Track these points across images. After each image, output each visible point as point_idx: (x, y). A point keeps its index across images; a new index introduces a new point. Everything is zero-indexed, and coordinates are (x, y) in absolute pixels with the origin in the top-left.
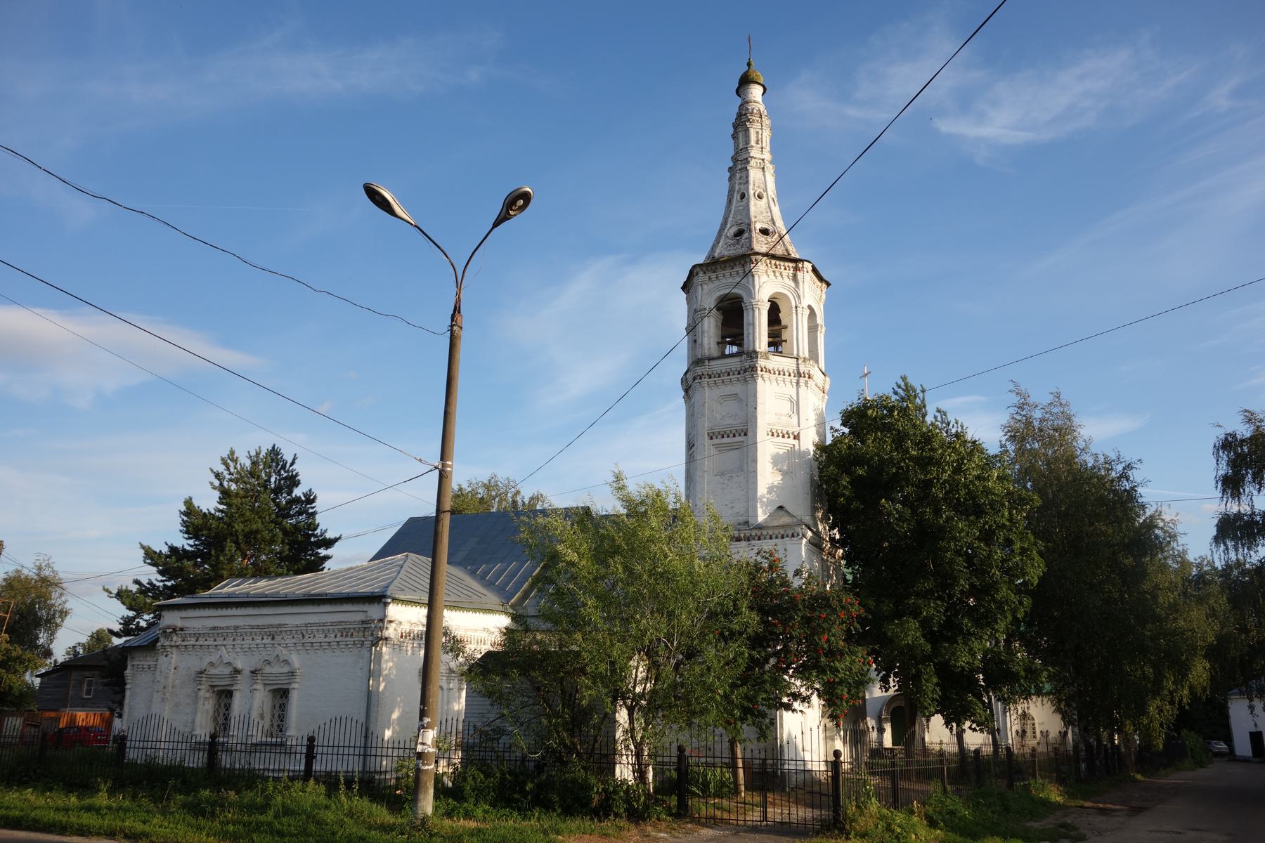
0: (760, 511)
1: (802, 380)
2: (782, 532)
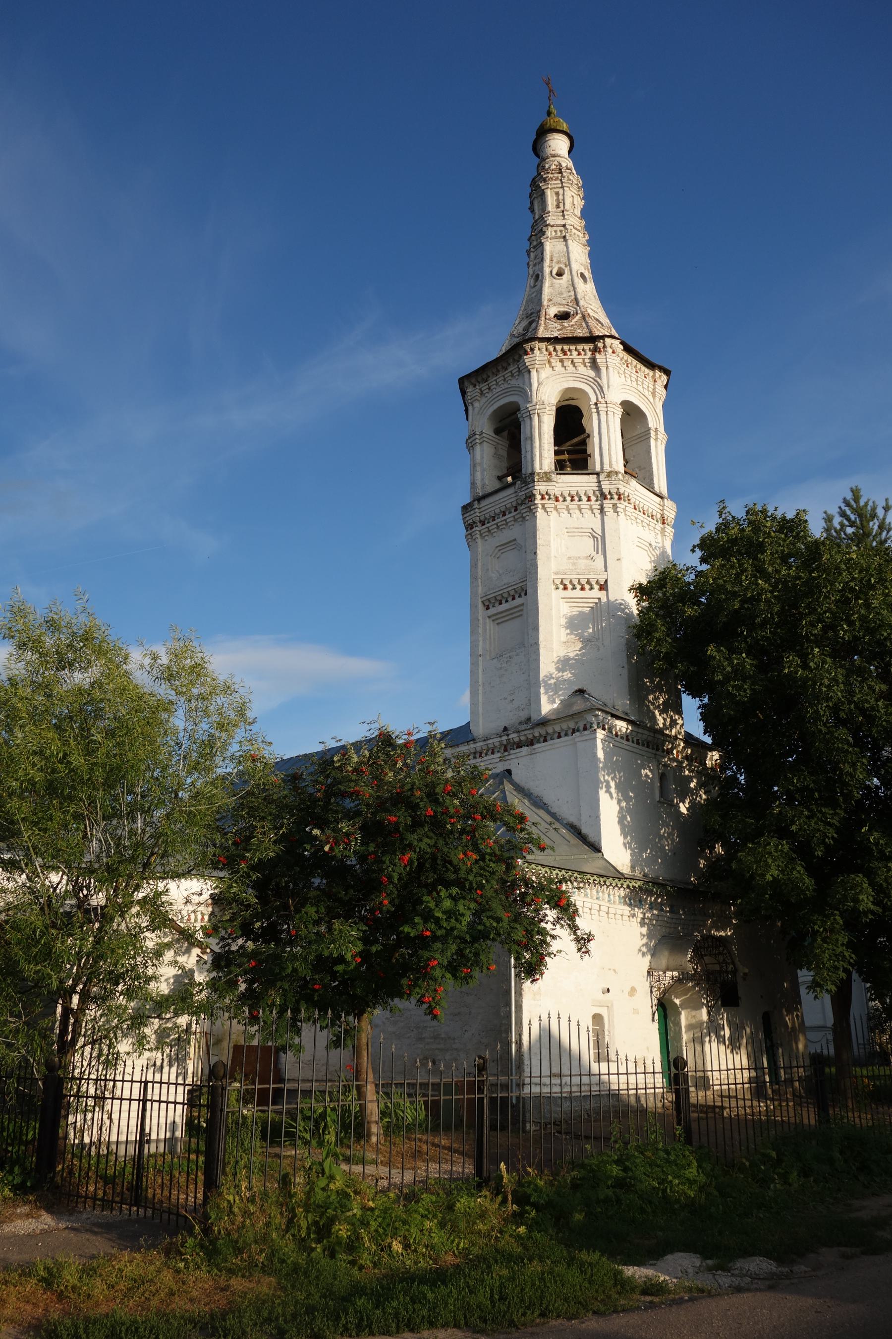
0: (544, 699)
1: (608, 504)
2: (572, 725)
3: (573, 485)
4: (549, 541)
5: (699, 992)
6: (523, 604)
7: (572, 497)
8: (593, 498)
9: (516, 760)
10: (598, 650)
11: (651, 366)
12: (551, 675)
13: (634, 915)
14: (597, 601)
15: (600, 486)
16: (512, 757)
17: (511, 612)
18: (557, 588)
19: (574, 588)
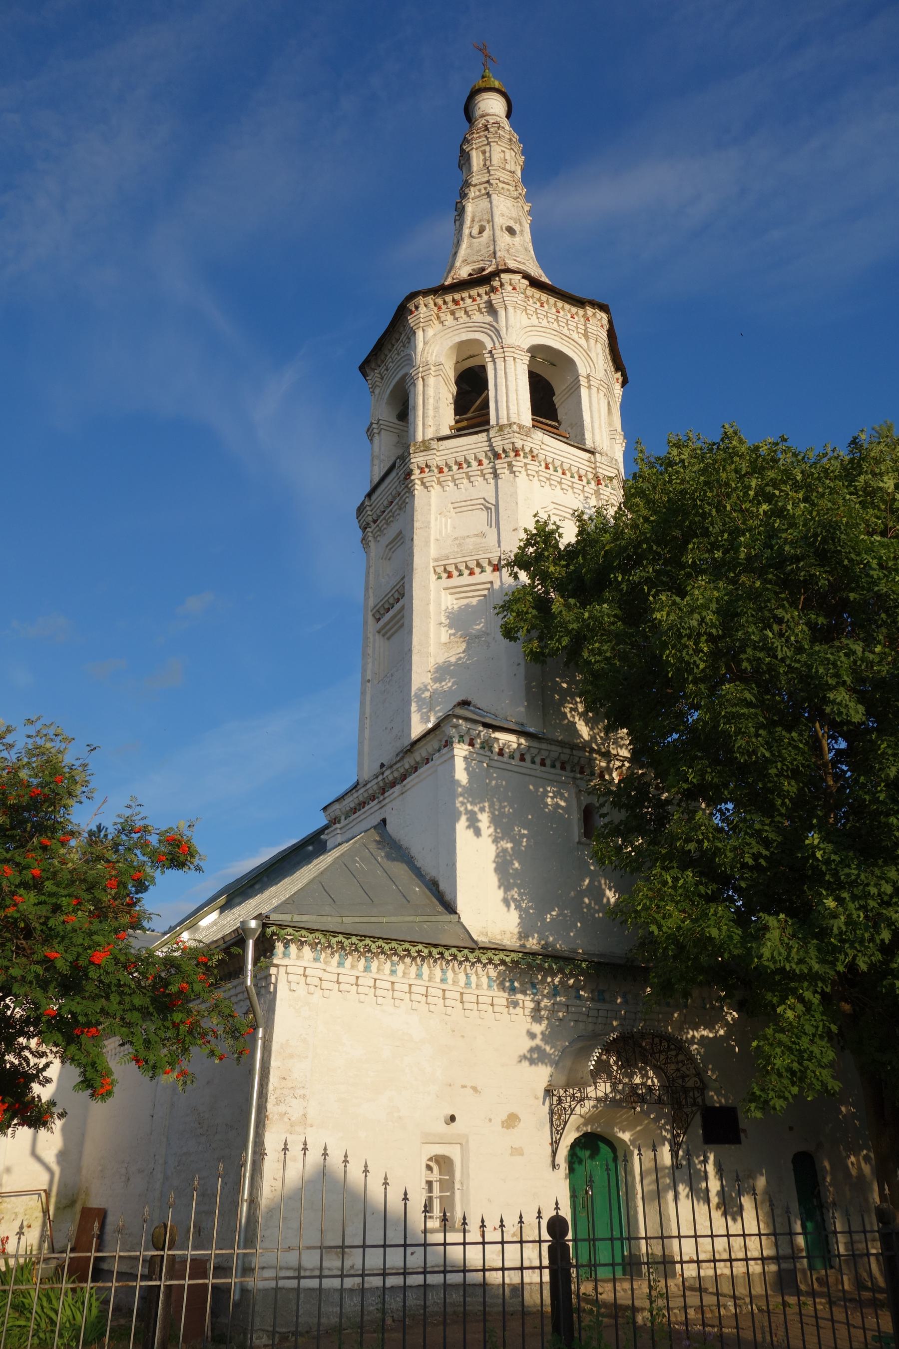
0: (415, 718)
1: (501, 464)
3: (458, 449)
4: (429, 522)
5: (657, 1119)
7: (460, 464)
8: (485, 462)
10: (488, 646)
11: (579, 302)
12: (426, 686)
13: (515, 1004)
14: (489, 586)
15: (491, 445)
16: (387, 801)
17: (396, 619)
18: (440, 578)
19: (461, 575)
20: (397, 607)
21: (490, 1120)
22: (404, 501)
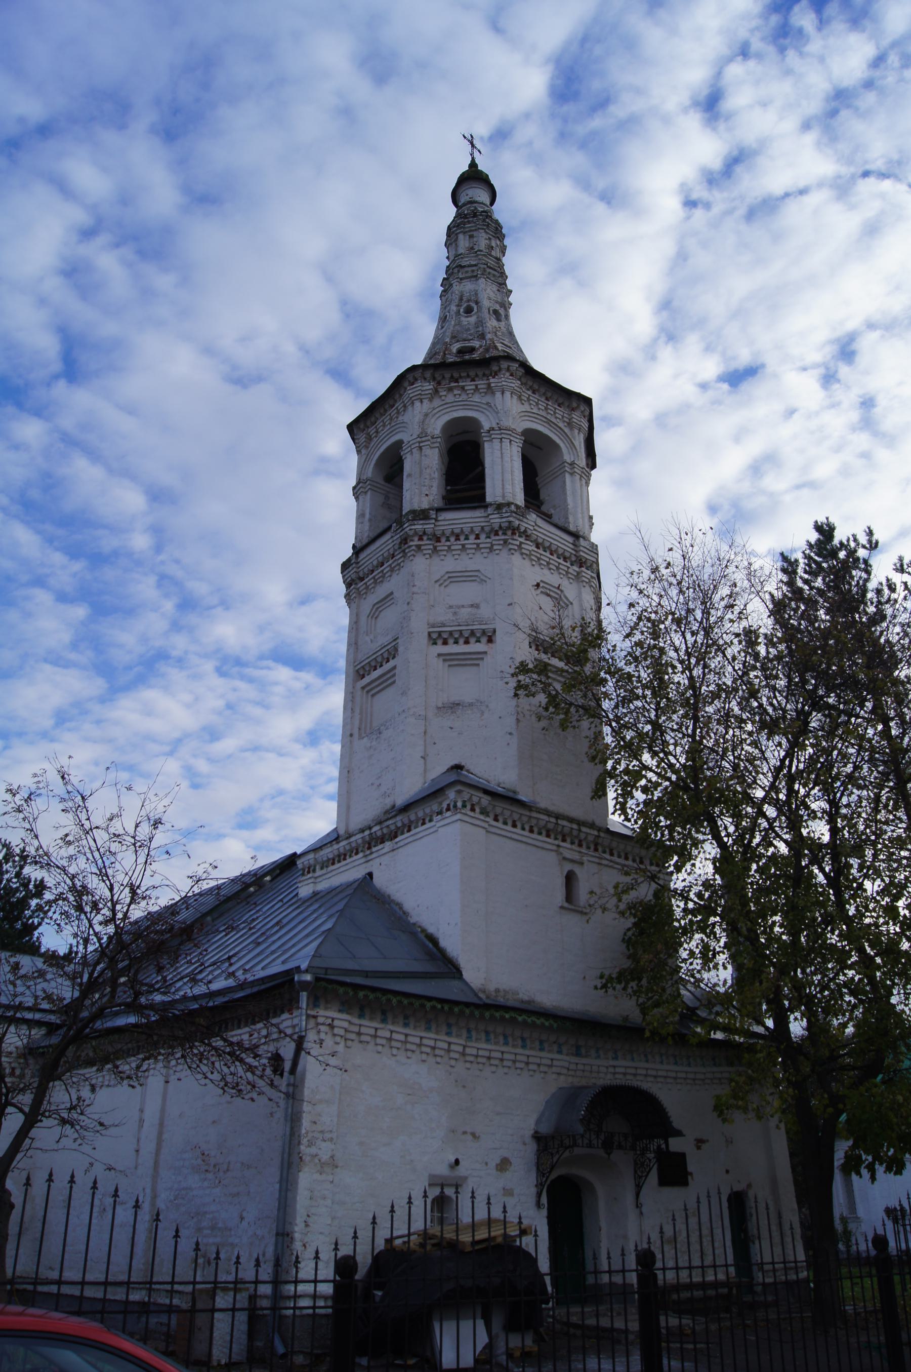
6: (485, 653)
9: (378, 860)
17: (385, 678)
20: (387, 666)
21: (486, 1164)
22: (399, 564)
